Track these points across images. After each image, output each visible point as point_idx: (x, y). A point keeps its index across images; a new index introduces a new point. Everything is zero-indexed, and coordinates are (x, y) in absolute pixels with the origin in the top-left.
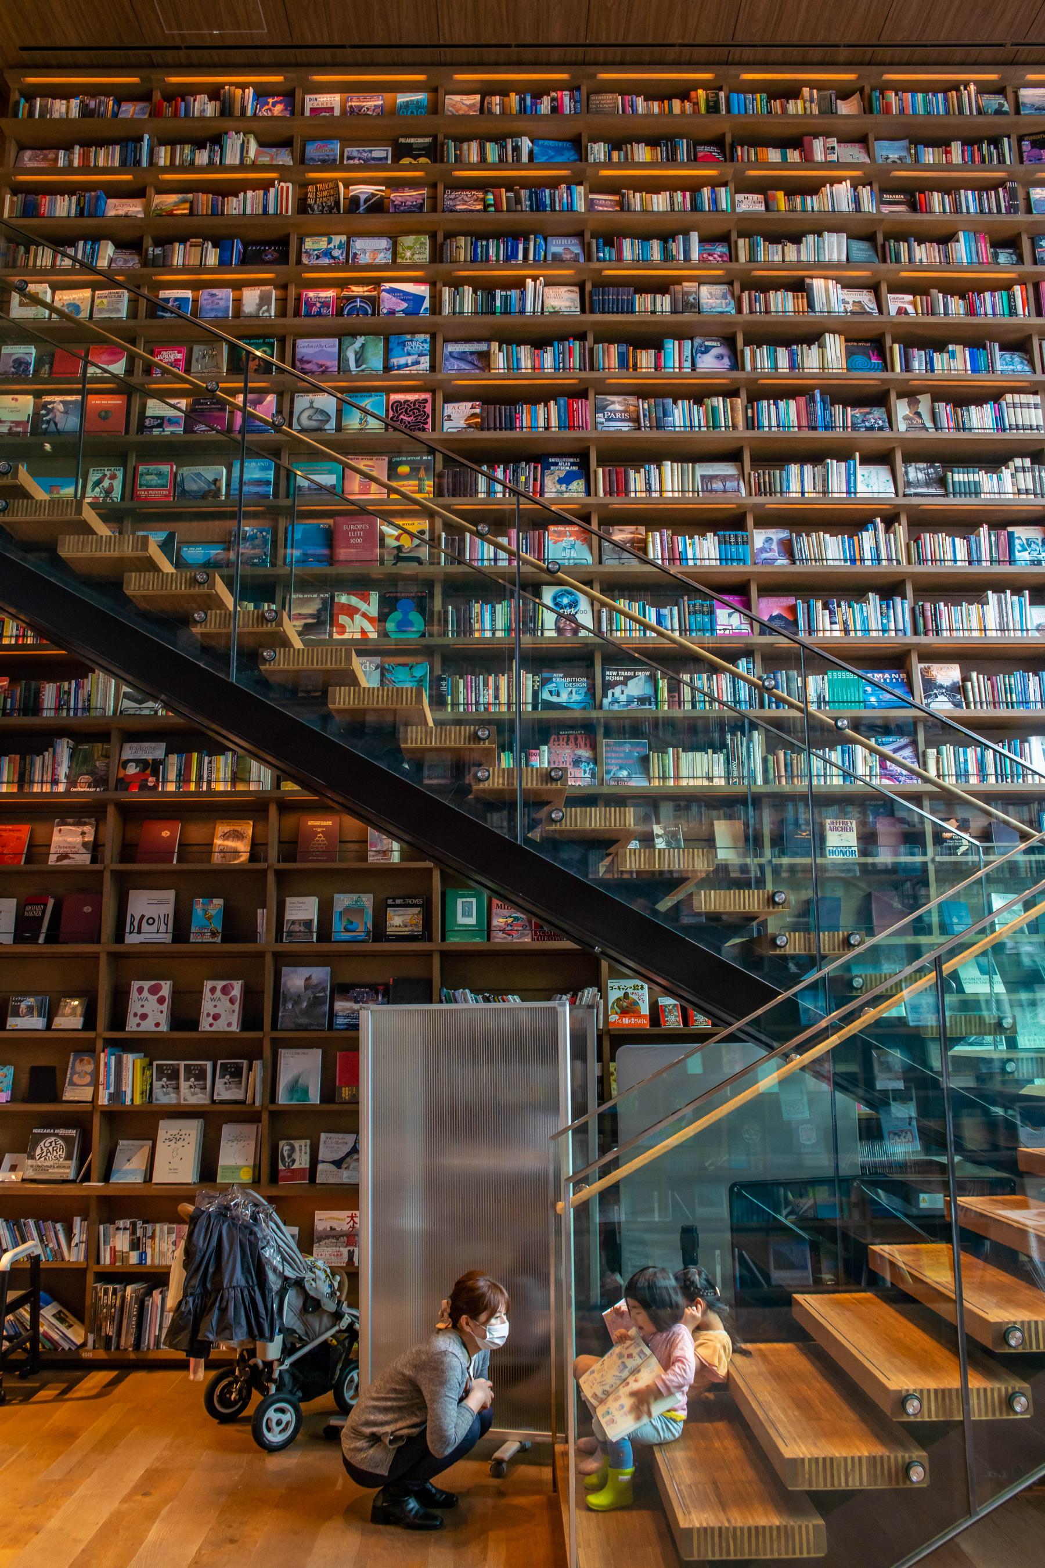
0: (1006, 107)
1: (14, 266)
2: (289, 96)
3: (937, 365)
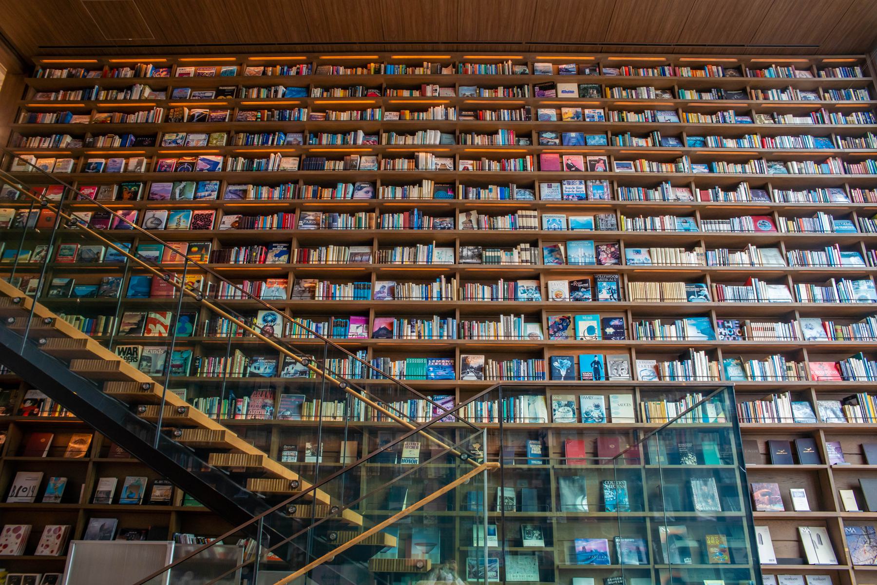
0: (527, 71)
1: (19, 146)
2: (170, 68)
3: (482, 196)
